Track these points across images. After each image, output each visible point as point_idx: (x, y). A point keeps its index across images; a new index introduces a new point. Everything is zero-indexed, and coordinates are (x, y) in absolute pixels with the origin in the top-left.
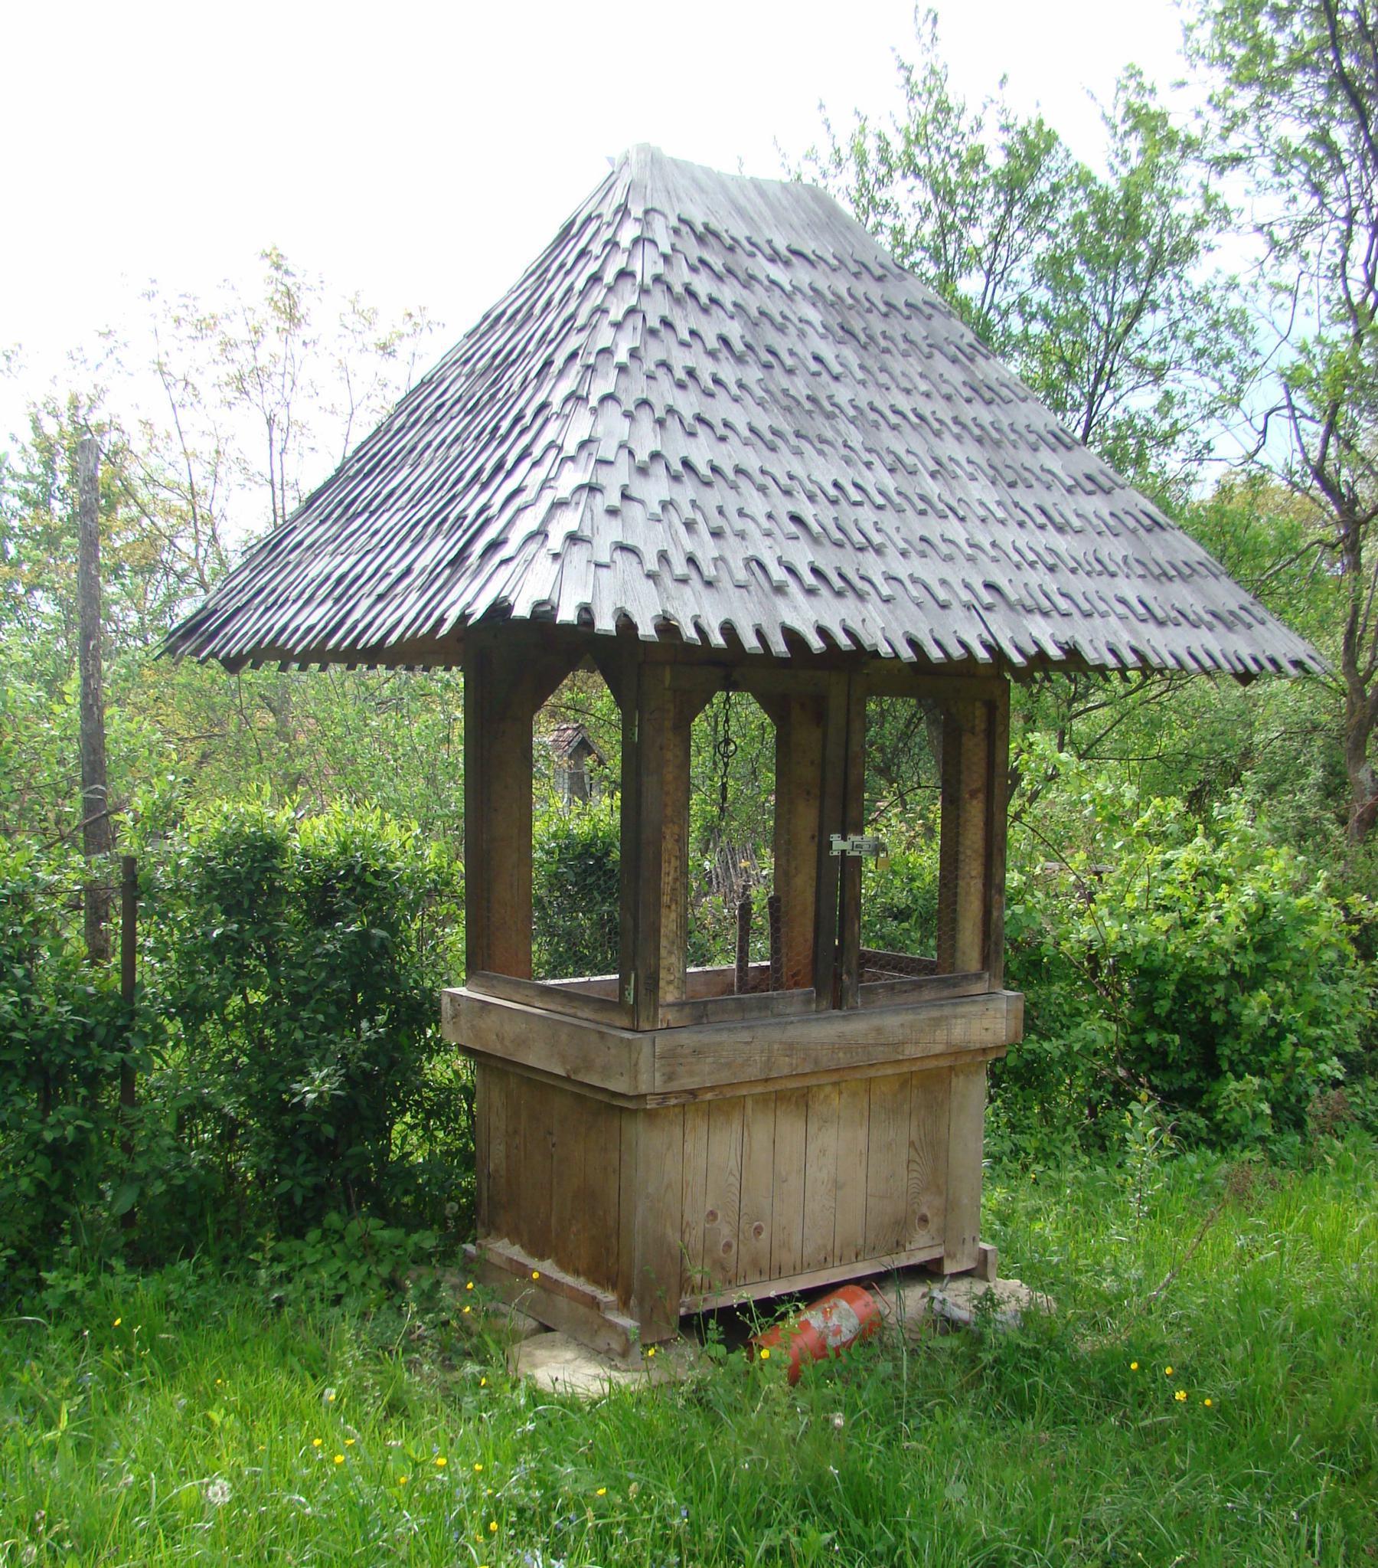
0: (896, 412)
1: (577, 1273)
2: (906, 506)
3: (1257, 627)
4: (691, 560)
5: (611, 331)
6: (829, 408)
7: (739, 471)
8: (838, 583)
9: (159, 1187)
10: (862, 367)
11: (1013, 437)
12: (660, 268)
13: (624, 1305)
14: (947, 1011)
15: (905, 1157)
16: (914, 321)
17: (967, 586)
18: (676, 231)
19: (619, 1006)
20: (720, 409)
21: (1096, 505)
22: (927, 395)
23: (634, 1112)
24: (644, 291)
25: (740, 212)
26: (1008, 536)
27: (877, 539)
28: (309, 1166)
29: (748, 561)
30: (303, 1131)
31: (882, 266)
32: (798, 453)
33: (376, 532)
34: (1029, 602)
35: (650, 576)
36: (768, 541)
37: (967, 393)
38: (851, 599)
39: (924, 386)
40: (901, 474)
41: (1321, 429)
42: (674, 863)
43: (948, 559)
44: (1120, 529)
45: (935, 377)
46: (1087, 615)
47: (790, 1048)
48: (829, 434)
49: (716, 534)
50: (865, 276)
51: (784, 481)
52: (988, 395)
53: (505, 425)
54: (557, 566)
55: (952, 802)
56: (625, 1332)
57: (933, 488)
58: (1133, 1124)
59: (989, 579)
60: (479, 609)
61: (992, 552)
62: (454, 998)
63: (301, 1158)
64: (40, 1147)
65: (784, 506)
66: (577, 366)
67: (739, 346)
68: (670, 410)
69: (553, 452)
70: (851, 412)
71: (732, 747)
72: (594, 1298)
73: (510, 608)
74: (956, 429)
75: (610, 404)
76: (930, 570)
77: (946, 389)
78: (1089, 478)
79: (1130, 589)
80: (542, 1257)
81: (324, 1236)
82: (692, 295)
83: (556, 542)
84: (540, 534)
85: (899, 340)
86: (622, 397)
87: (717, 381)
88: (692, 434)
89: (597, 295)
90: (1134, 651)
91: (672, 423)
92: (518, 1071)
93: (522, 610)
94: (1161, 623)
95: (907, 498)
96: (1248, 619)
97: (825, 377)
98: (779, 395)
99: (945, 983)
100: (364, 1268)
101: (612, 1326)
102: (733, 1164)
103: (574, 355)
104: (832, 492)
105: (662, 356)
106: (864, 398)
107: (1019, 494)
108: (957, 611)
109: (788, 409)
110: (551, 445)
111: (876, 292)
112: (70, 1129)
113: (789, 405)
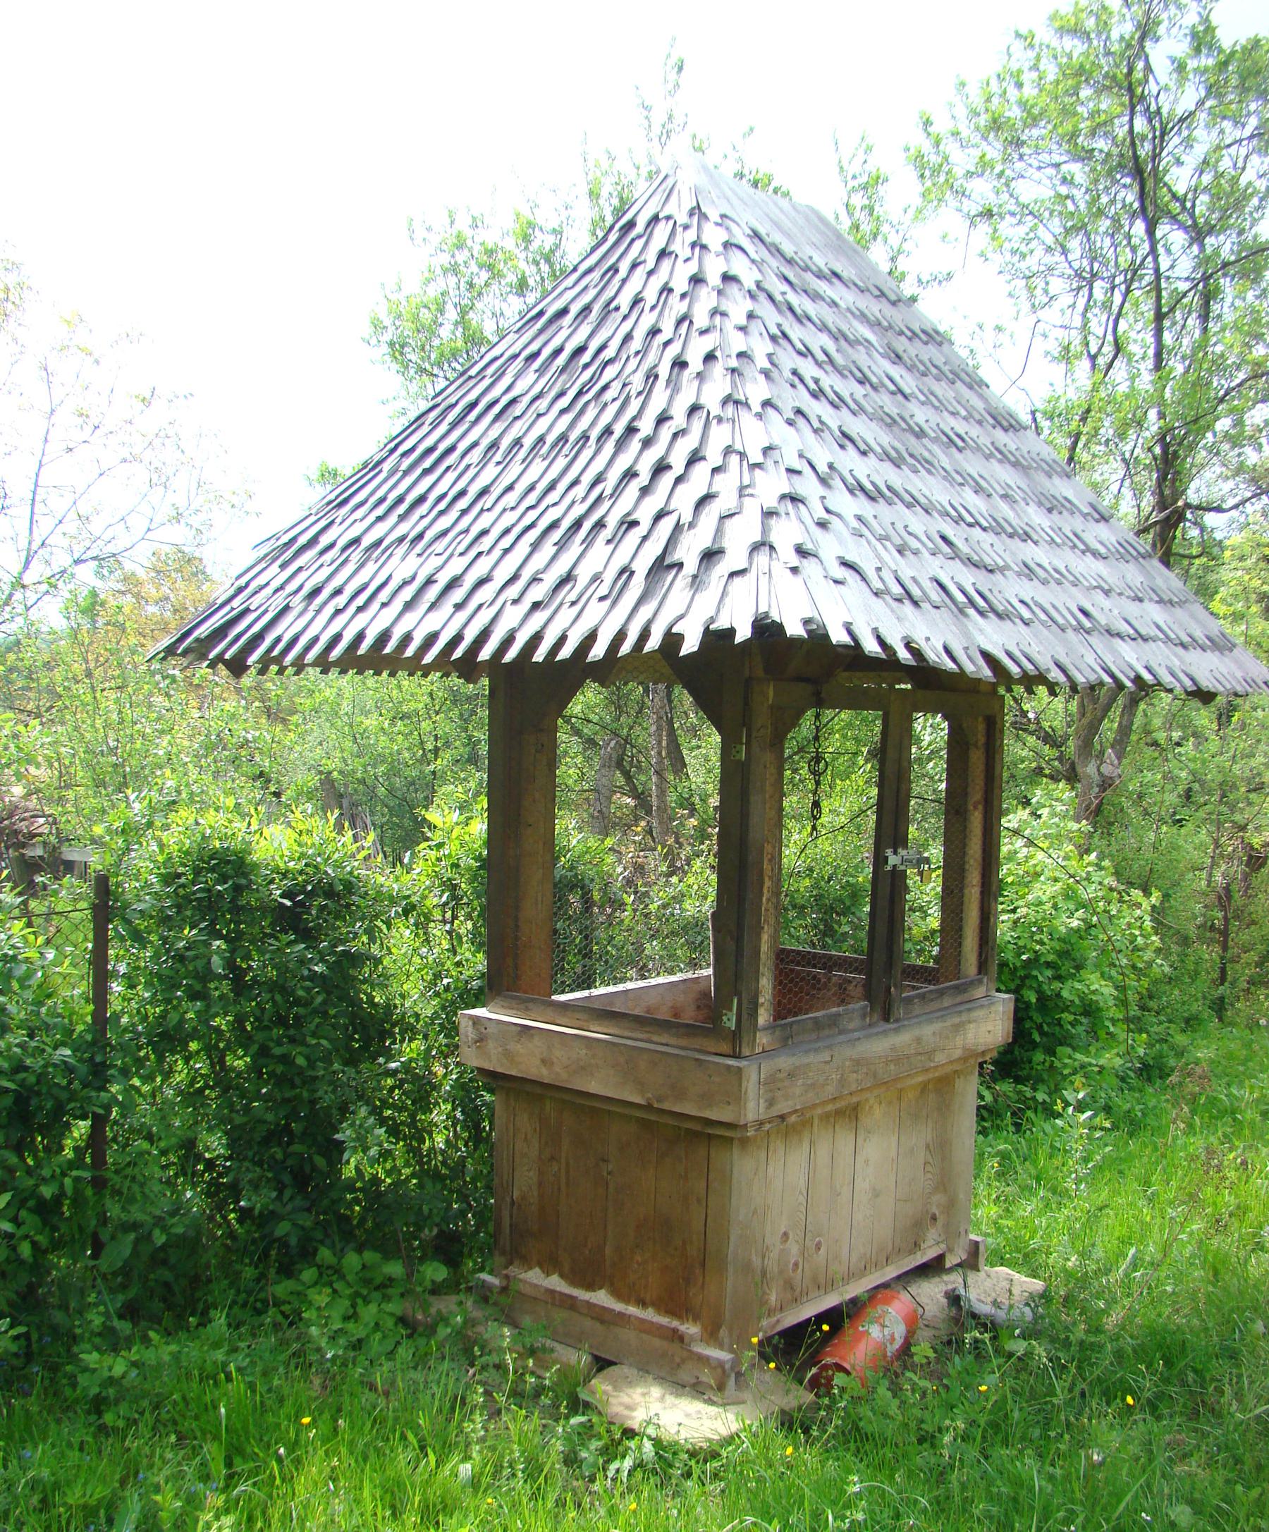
1: (642, 1303)
13: (711, 1335)
14: (964, 1017)
15: (922, 1161)
33: (484, 533)
44: (1129, 558)
47: (857, 1062)
55: (957, 812)
56: (721, 1364)
58: (1064, 1109)
62: (476, 1021)
64: (31, 1203)
66: (718, 369)
69: (734, 459)
71: (822, 765)
72: (675, 1331)
73: (779, 627)
80: (591, 1287)
84: (762, 545)
101: (703, 1360)
110: (728, 451)
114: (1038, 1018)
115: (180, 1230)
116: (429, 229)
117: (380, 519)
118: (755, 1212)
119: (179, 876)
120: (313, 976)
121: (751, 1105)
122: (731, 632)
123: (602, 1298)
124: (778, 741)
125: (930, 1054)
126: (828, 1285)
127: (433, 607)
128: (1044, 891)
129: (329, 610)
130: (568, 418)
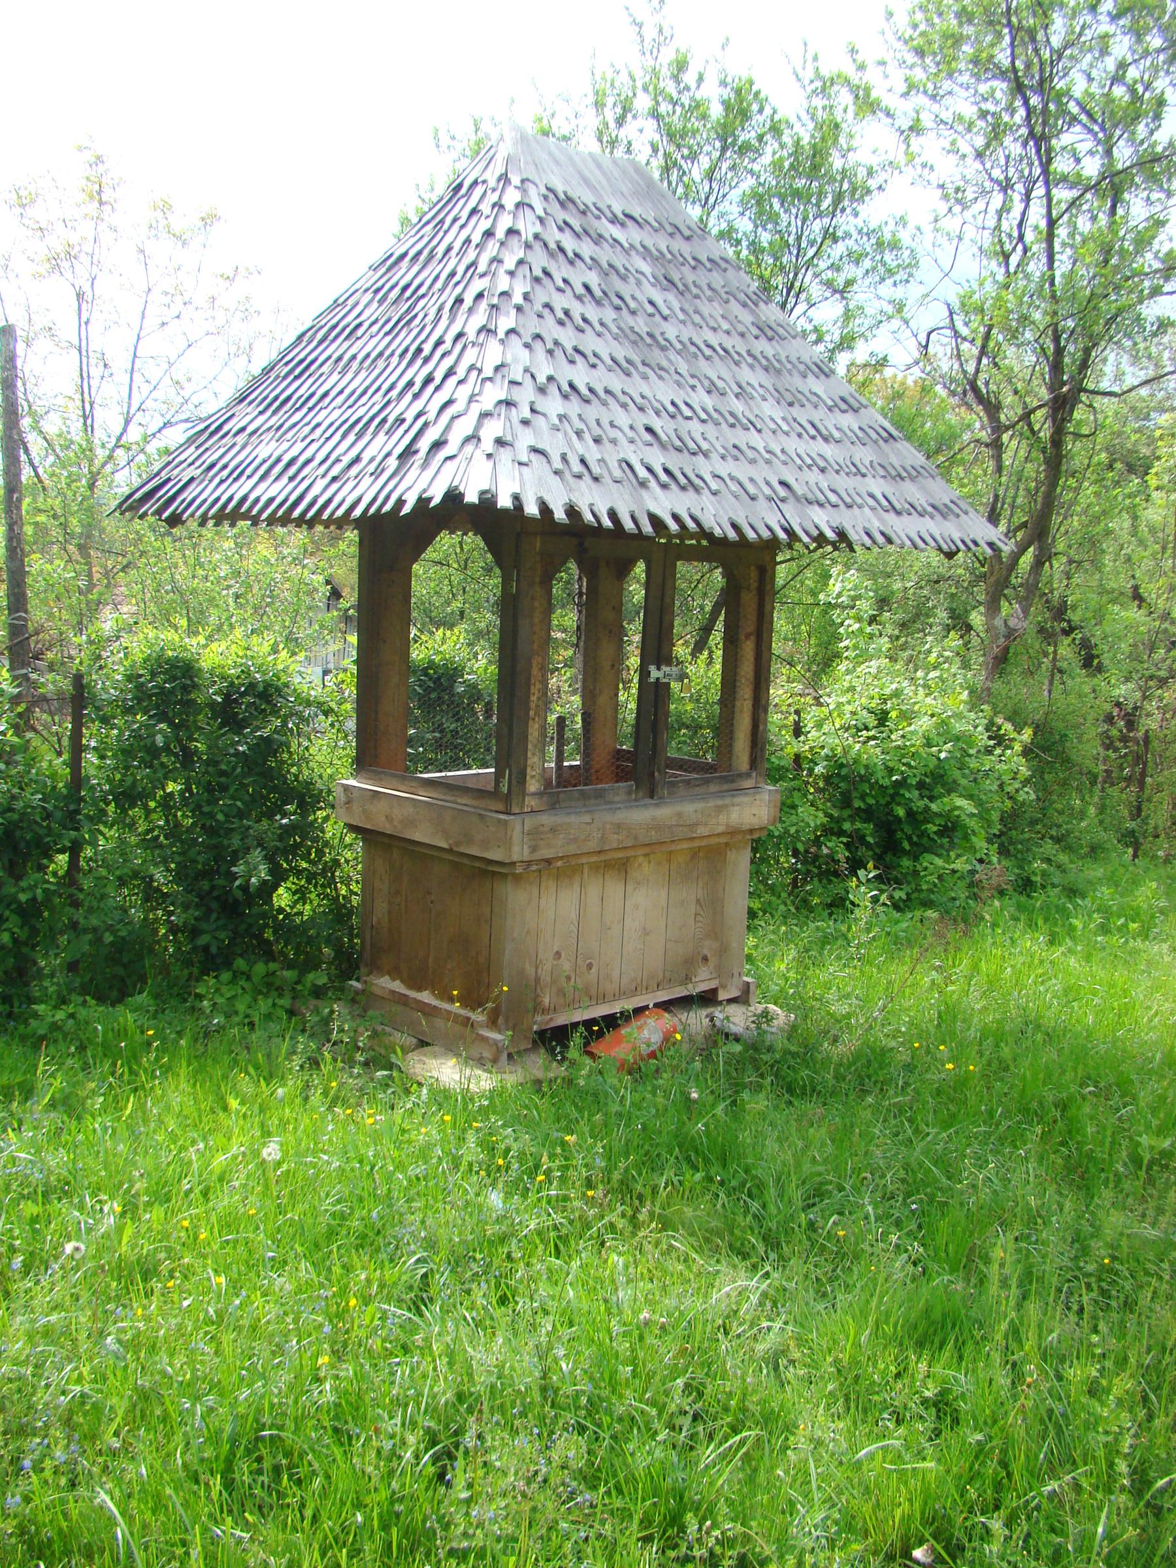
0: (708, 346)
2: (721, 420)
3: (963, 515)
4: (583, 461)
5: (507, 278)
6: (663, 343)
7: (607, 391)
8: (683, 481)
9: (108, 938)
10: (682, 310)
11: (789, 366)
12: (538, 228)
13: (493, 1023)
14: (727, 801)
16: (714, 273)
17: (768, 483)
18: (546, 198)
19: (495, 794)
20: (590, 343)
21: (848, 421)
22: (728, 333)
23: (504, 876)
24: (528, 246)
25: (586, 181)
26: (793, 445)
27: (705, 446)
28: (221, 922)
29: (620, 461)
30: (216, 893)
31: (689, 228)
32: (645, 377)
33: (318, 425)
34: (810, 496)
35: (557, 473)
36: (632, 447)
37: (755, 331)
38: (691, 493)
39: (725, 326)
40: (715, 394)
41: (975, 351)
42: (538, 686)
43: (753, 462)
44: (866, 440)
45: (732, 318)
46: (849, 507)
47: (618, 827)
48: (665, 364)
49: (597, 441)
50: (678, 236)
51: (639, 400)
52: (770, 333)
53: (427, 349)
54: (491, 463)
55: (732, 642)
56: (496, 1042)
57: (738, 407)
59: (783, 478)
60: (437, 495)
61: (783, 458)
63: (214, 916)
64: (14, 906)
65: (641, 420)
66: (483, 305)
67: (598, 293)
68: (556, 343)
69: (474, 373)
70: (679, 346)
72: (468, 1019)
73: (462, 495)
74: (750, 360)
75: (513, 336)
76: (742, 471)
77: (741, 328)
78: (843, 399)
79: (877, 486)
80: (419, 989)
81: (235, 976)
82: (562, 250)
83: (488, 445)
84: (473, 438)
85: (705, 288)
86: (522, 331)
87: (585, 320)
88: (572, 362)
89: (492, 248)
90: (883, 534)
91: (558, 353)
92: (402, 844)
93: (471, 497)
94: (898, 513)
95: (720, 414)
96: (957, 510)
97: (658, 317)
98: (628, 332)
99: (726, 780)
100: (270, 1001)
101: (484, 1039)
102: (573, 916)
103: (480, 296)
104: (671, 409)
105: (545, 300)
106: (687, 333)
107: (796, 411)
108: (762, 502)
109: (634, 343)
110: (472, 368)
111: (686, 249)
112: (39, 891)
113: (635, 339)
114: (908, 830)
115: (123, 933)
116: (453, 138)
117: (261, 413)
118: (528, 932)
119: (141, 676)
120: (237, 754)
121: (516, 849)
122: (430, 499)
123: (425, 997)
124: (547, 581)
125: (693, 826)
126: (603, 998)
127: (277, 479)
128: (923, 724)
129: (217, 480)
130: (388, 338)
